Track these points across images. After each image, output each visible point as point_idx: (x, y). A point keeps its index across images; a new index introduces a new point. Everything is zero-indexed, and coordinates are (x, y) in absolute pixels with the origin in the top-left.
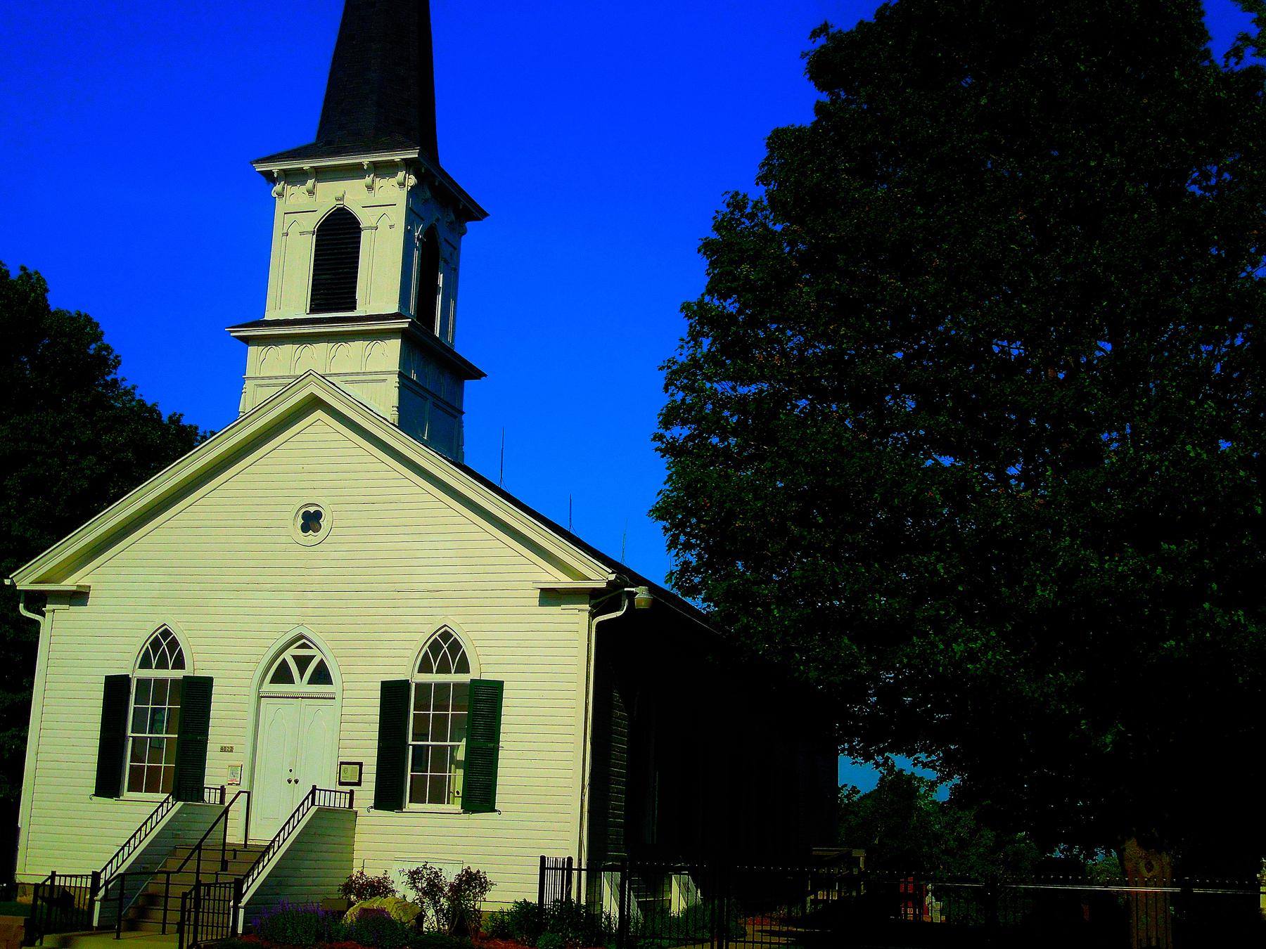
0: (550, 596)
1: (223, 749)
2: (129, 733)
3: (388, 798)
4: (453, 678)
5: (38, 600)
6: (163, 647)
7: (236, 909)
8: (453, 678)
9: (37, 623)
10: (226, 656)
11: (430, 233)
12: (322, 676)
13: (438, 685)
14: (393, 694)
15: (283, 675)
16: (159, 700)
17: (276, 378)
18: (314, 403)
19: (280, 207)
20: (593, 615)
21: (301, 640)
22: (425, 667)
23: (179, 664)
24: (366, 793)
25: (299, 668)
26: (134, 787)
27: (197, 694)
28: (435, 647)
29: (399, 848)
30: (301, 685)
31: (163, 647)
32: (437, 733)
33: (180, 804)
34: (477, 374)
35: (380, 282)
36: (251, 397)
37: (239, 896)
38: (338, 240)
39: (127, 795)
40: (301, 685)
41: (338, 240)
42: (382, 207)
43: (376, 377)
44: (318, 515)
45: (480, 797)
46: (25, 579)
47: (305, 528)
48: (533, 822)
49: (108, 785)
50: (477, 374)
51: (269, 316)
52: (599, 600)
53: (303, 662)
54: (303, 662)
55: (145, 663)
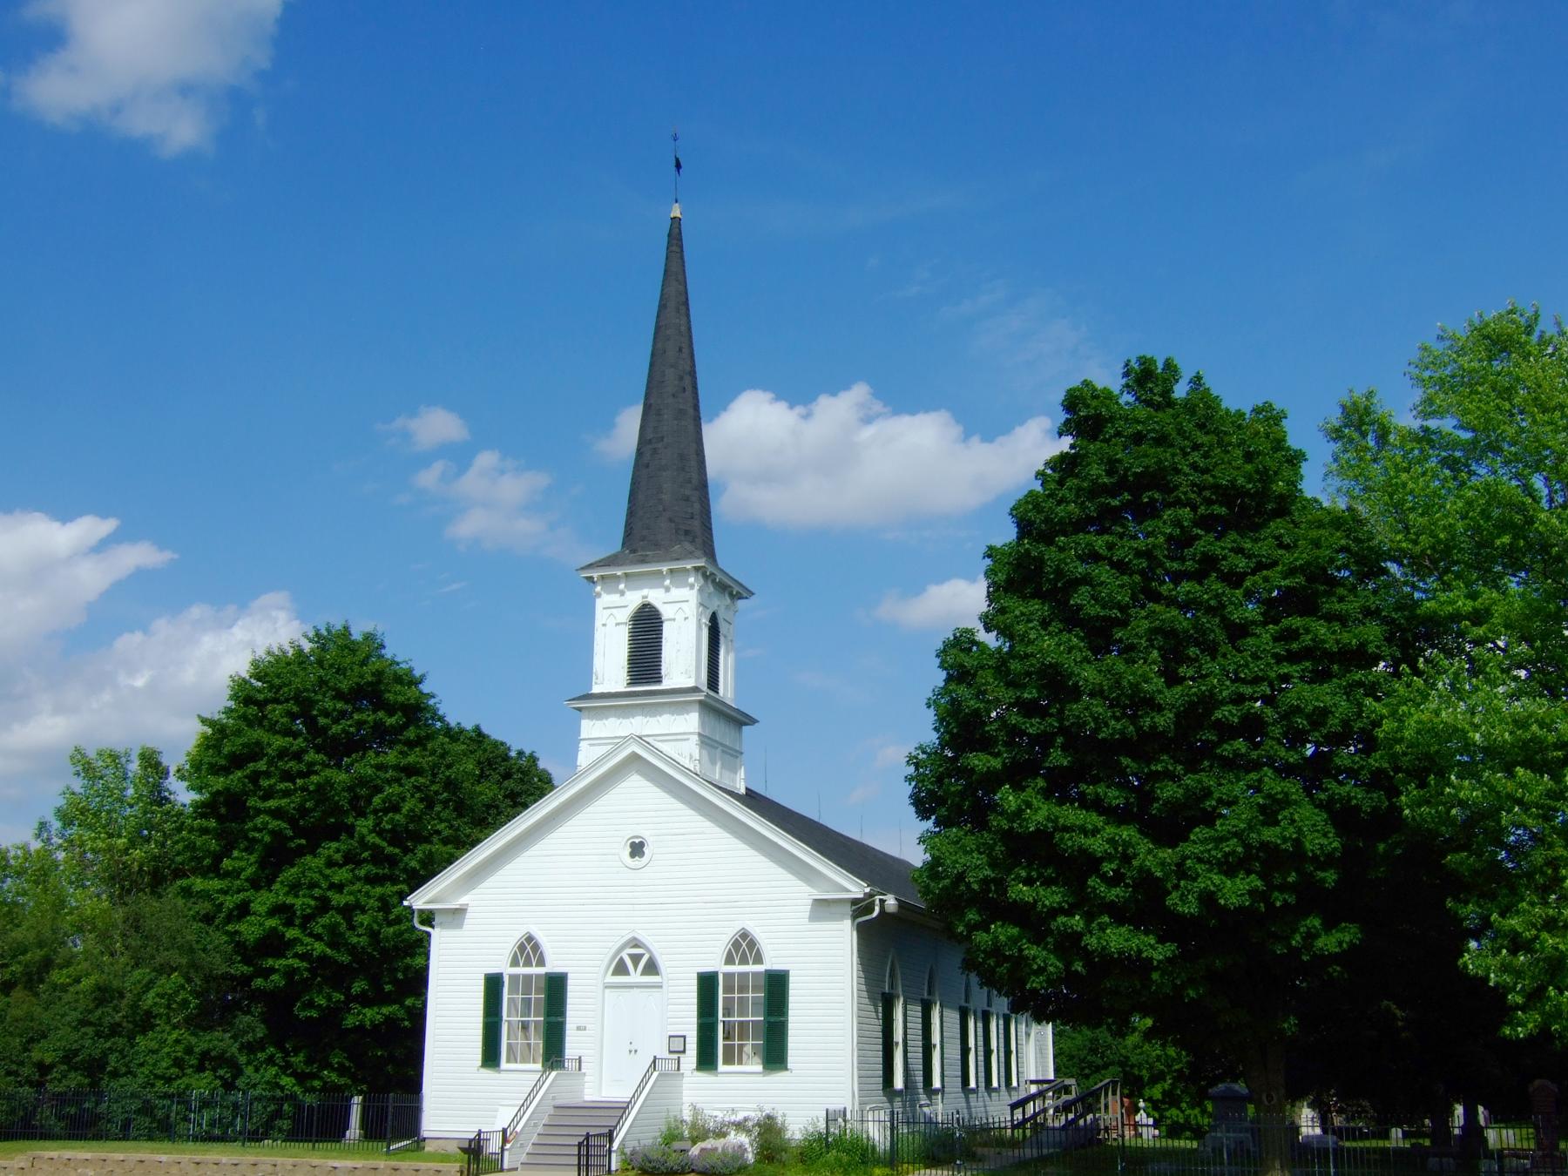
0: (823, 908)
1: (579, 1028)
2: (505, 1017)
3: (706, 1060)
4: (751, 968)
5: (428, 918)
6: (529, 949)
7: (610, 1151)
8: (751, 968)
9: (429, 935)
10: (578, 957)
11: (714, 619)
12: (652, 968)
13: (740, 974)
14: (707, 984)
15: (621, 969)
16: (527, 991)
17: (965, 1051)
18: (635, 757)
19: (600, 603)
20: (854, 917)
21: (636, 943)
22: (729, 960)
23: (541, 962)
24: (691, 1057)
25: (636, 962)
26: (729, 1060)
27: (556, 987)
28: (736, 945)
29: (734, 1096)
30: (635, 976)
31: (529, 949)
32: (744, 1014)
33: (554, 1074)
34: (753, 721)
35: (681, 660)
36: (586, 755)
37: (611, 1141)
38: (647, 626)
39: (721, 1067)
40: (635, 976)
41: (647, 626)
42: (681, 608)
43: (679, 737)
44: (642, 845)
45: (775, 1055)
46: (419, 900)
47: (633, 855)
48: (823, 1077)
49: (491, 1056)
50: (753, 721)
51: (596, 690)
52: (860, 908)
53: (636, 959)
54: (636, 959)
55: (515, 963)
